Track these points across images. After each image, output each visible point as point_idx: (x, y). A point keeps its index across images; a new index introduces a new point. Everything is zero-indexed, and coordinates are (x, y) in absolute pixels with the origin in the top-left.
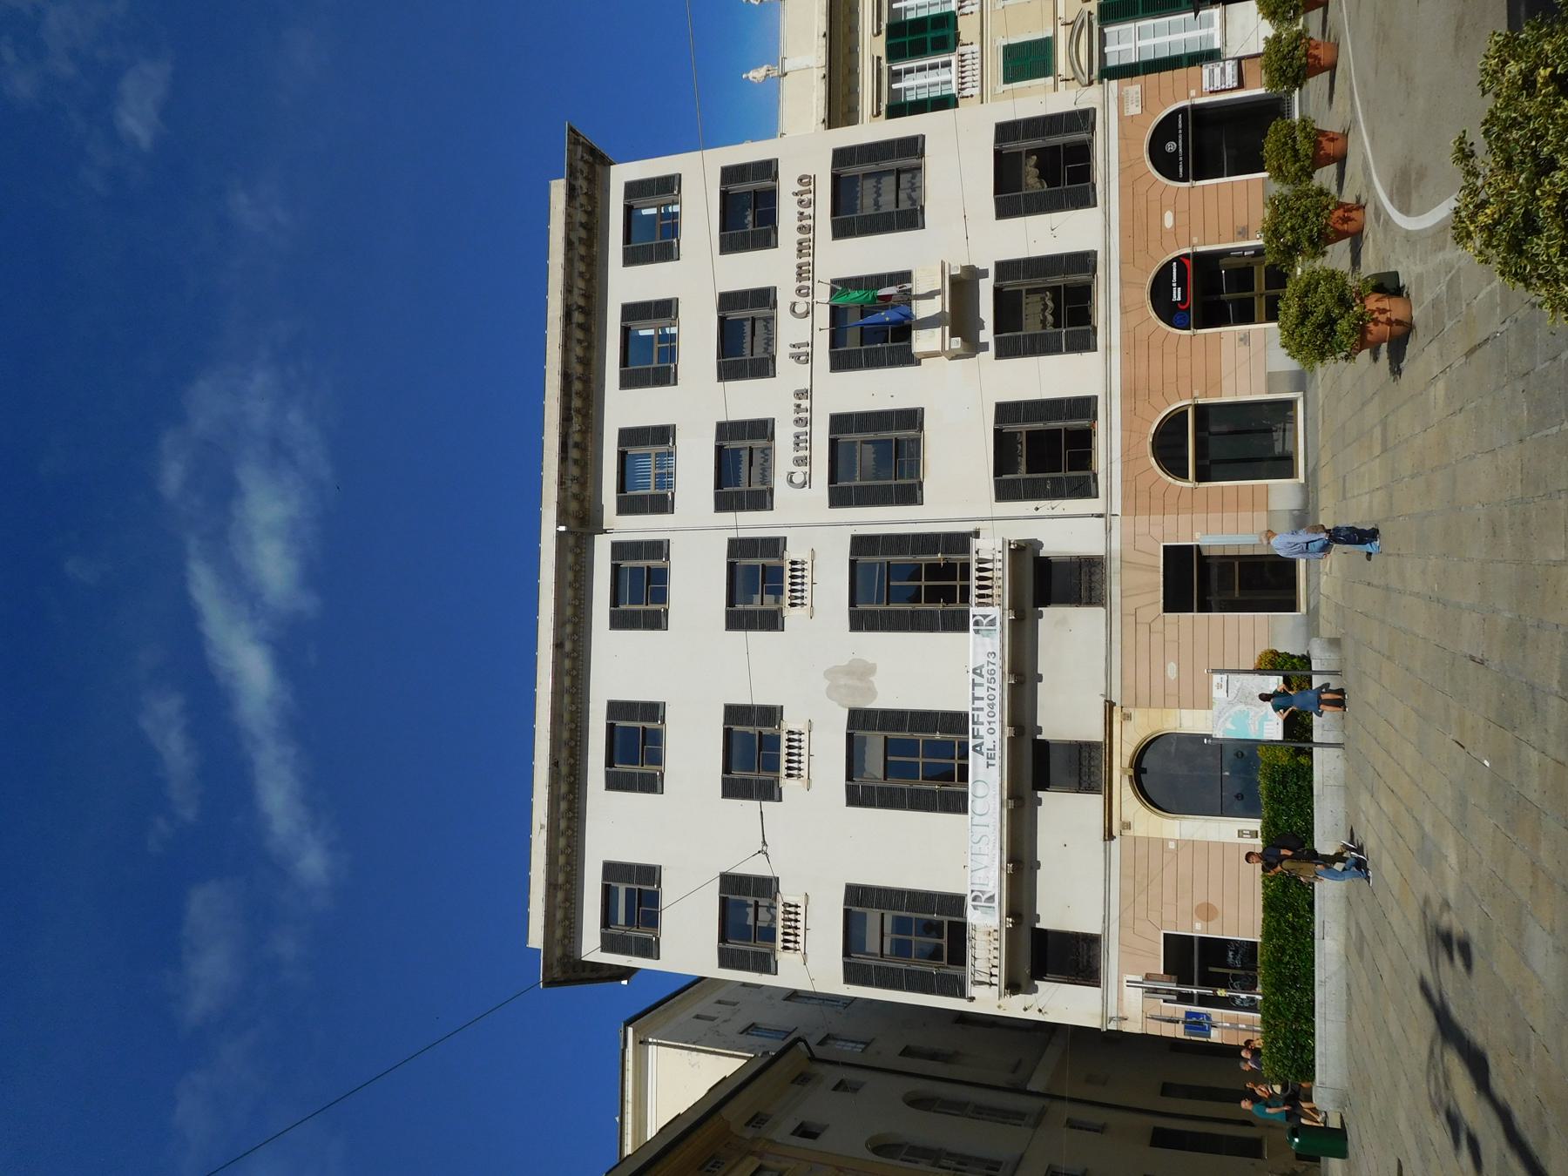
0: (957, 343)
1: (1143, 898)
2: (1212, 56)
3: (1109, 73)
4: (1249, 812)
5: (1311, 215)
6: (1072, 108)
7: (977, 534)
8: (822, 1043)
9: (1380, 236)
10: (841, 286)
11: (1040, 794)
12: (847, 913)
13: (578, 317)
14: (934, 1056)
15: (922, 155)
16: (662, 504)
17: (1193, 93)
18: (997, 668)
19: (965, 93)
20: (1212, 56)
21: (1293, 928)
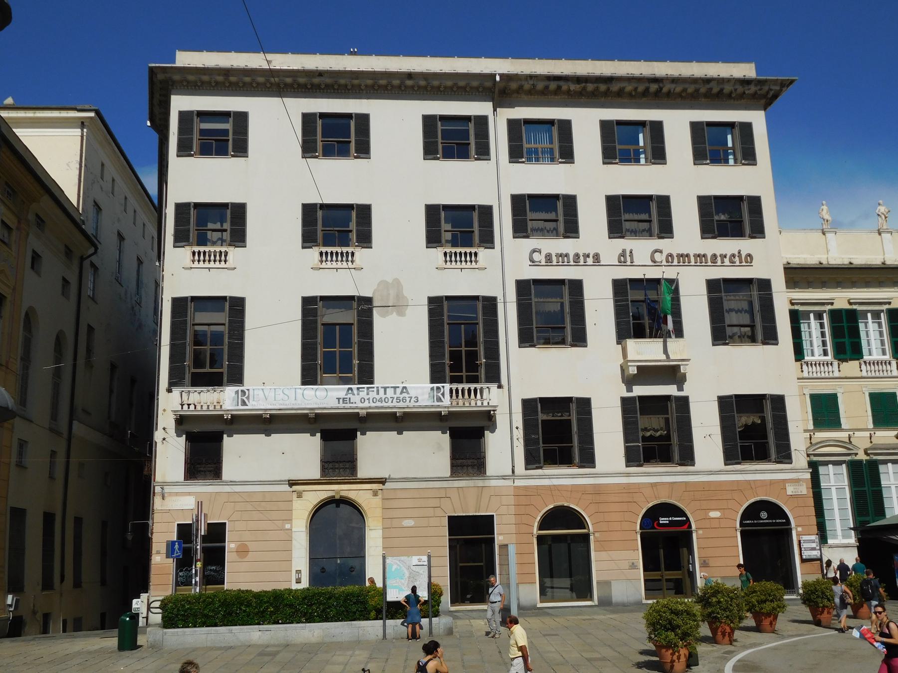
0: (633, 370)
1: (249, 507)
2: (823, 539)
3: (814, 467)
4: (314, 578)
5: (728, 613)
6: (793, 447)
7: (500, 387)
8: (93, 265)
9: (716, 655)
10: (673, 284)
11: (318, 435)
12: (224, 298)
13: (654, 87)
14: (89, 351)
15: (764, 343)
16: (516, 154)
17: (800, 529)
18: (407, 403)
19: (805, 367)
20: (823, 539)
21: (264, 611)
